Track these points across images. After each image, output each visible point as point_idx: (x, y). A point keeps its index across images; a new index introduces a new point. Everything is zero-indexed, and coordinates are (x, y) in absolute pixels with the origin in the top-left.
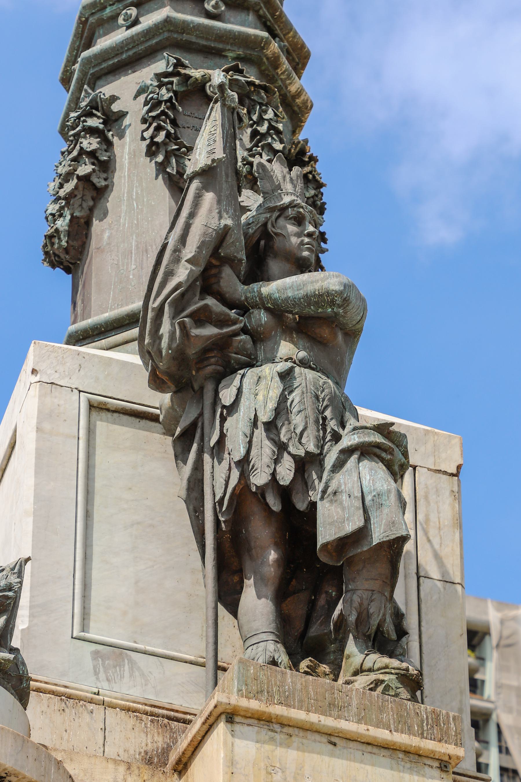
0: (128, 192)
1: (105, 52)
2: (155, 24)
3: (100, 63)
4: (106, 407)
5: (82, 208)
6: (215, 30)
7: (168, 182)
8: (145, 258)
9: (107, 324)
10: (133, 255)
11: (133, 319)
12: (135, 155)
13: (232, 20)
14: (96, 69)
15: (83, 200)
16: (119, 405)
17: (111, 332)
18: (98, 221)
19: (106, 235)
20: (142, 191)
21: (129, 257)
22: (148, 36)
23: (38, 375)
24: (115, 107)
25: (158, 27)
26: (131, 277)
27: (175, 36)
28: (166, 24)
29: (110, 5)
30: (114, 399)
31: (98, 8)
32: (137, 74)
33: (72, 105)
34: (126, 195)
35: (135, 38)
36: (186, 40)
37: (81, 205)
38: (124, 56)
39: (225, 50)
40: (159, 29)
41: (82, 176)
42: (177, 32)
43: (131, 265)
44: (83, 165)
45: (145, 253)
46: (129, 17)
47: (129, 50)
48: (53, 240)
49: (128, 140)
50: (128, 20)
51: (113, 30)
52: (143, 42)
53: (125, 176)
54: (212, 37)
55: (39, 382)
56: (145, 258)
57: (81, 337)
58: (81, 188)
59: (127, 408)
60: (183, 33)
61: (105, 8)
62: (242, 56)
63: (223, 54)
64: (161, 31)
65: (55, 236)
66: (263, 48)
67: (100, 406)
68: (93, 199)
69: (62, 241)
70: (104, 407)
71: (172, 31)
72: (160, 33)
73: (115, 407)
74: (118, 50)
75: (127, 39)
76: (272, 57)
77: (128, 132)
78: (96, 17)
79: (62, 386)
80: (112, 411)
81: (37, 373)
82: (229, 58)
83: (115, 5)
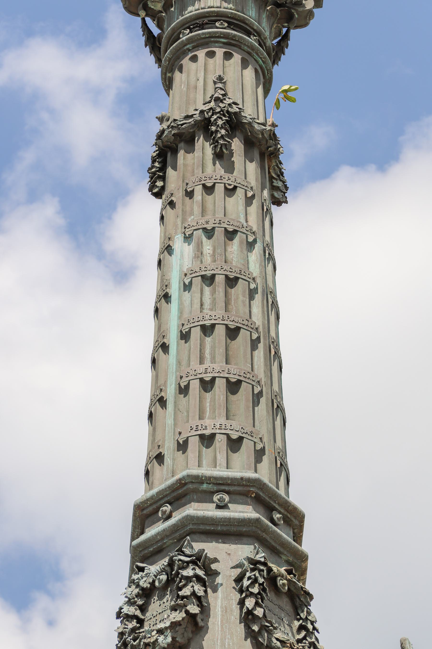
0: (221, 639)
2: (249, 519)
20: (233, 644)
22: (240, 524)
27: (260, 532)
28: (257, 522)
29: (207, 483)
31: (198, 481)
33: (158, 537)
34: (219, 642)
35: (231, 520)
37: (183, 634)
38: (219, 528)
39: (283, 554)
40: (250, 523)
41: (191, 614)
42: (261, 530)
46: (223, 500)
49: (220, 595)
54: (279, 542)
58: (186, 621)
60: (263, 532)
61: (203, 483)
63: (280, 555)
64: (251, 525)
68: (193, 632)
71: (258, 528)
72: (250, 526)
74: (216, 522)
75: (226, 518)
76: (304, 568)
77: (220, 589)
78: (195, 486)
82: (283, 559)
83: (211, 485)
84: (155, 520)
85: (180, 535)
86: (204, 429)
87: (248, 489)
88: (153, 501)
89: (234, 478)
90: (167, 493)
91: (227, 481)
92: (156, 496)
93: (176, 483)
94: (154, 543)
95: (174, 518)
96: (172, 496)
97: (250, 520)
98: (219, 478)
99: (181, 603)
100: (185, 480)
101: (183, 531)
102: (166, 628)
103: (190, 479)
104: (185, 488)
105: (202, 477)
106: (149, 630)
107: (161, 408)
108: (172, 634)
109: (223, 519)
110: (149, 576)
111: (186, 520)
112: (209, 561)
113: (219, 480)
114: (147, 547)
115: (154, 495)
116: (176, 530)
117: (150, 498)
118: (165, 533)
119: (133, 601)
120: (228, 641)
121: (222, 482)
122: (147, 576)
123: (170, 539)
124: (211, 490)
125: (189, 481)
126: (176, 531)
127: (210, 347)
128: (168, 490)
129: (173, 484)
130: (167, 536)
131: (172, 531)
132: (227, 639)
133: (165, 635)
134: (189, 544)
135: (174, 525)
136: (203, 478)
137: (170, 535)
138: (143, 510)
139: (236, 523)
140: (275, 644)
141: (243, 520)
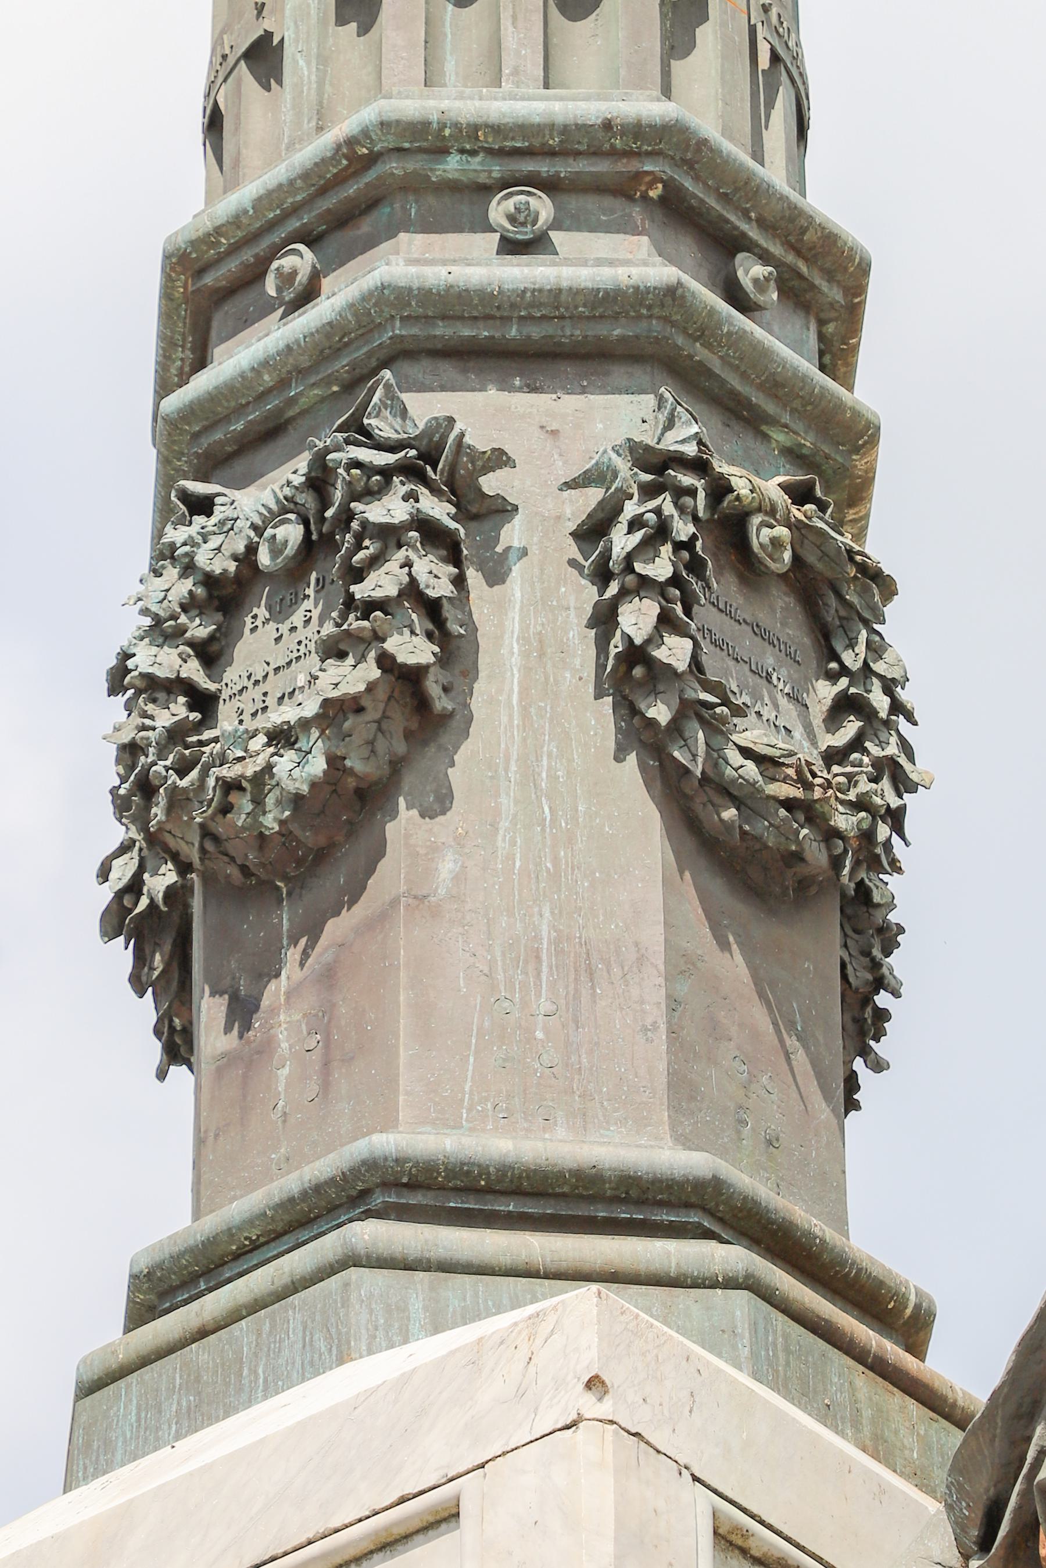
1: (459, 295)
2: (637, 288)
3: (426, 317)
4: (744, 1545)
5: (373, 751)
6: (772, 361)
7: (658, 784)
8: (585, 993)
9: (505, 1175)
10: (545, 969)
11: (585, 1188)
12: (542, 655)
13: (776, 328)
14: (415, 331)
15: (380, 729)
16: (776, 1547)
17: (503, 1199)
18: (415, 812)
19: (447, 867)
21: (531, 968)
22: (601, 310)
23: (608, 1401)
24: (490, 483)
25: (643, 299)
26: (539, 1035)
27: (680, 340)
28: (668, 301)
29: (462, 151)
30: (762, 1522)
32: (543, 400)
33: (266, 377)
34: (513, 767)
36: (700, 362)
37: (371, 743)
38: (513, 332)
40: (641, 305)
42: (684, 331)
43: (539, 995)
44: (406, 631)
45: (584, 977)
50: (523, 224)
51: (458, 228)
53: (510, 706)
55: (612, 1422)
56: (585, 993)
57: (405, 1180)
58: (382, 694)
59: (790, 1562)
60: (696, 339)
61: (444, 151)
62: (804, 451)
63: (764, 428)
64: (644, 311)
65: (243, 789)
66: (857, 450)
67: (733, 1538)
68: (408, 735)
69: (264, 813)
70: (740, 1542)
71: (673, 324)
72: (639, 317)
73: (765, 1549)
74: (498, 308)
76: (860, 477)
78: (412, 165)
79: (658, 1452)
80: (752, 1557)
81: (606, 1392)
82: (774, 445)
88: (240, 234)
89: (576, 125)
90: (299, 198)
92: (251, 212)
93: (333, 158)
94: (248, 403)
98: (511, 129)
101: (365, 349)
104: (371, 176)
106: (239, 734)
108: (328, 743)
109: (528, 294)
111: (375, 305)
113: (511, 135)
115: (245, 212)
118: (291, 360)
121: (527, 144)
122: (225, 529)
123: (314, 384)
124: (480, 181)
125: (386, 144)
126: (337, 351)
128: (302, 188)
129: (322, 163)
130: (302, 372)
131: (322, 352)
132: (545, 758)
134: (392, 400)
135: (328, 328)
138: (201, 272)
141: (611, 294)
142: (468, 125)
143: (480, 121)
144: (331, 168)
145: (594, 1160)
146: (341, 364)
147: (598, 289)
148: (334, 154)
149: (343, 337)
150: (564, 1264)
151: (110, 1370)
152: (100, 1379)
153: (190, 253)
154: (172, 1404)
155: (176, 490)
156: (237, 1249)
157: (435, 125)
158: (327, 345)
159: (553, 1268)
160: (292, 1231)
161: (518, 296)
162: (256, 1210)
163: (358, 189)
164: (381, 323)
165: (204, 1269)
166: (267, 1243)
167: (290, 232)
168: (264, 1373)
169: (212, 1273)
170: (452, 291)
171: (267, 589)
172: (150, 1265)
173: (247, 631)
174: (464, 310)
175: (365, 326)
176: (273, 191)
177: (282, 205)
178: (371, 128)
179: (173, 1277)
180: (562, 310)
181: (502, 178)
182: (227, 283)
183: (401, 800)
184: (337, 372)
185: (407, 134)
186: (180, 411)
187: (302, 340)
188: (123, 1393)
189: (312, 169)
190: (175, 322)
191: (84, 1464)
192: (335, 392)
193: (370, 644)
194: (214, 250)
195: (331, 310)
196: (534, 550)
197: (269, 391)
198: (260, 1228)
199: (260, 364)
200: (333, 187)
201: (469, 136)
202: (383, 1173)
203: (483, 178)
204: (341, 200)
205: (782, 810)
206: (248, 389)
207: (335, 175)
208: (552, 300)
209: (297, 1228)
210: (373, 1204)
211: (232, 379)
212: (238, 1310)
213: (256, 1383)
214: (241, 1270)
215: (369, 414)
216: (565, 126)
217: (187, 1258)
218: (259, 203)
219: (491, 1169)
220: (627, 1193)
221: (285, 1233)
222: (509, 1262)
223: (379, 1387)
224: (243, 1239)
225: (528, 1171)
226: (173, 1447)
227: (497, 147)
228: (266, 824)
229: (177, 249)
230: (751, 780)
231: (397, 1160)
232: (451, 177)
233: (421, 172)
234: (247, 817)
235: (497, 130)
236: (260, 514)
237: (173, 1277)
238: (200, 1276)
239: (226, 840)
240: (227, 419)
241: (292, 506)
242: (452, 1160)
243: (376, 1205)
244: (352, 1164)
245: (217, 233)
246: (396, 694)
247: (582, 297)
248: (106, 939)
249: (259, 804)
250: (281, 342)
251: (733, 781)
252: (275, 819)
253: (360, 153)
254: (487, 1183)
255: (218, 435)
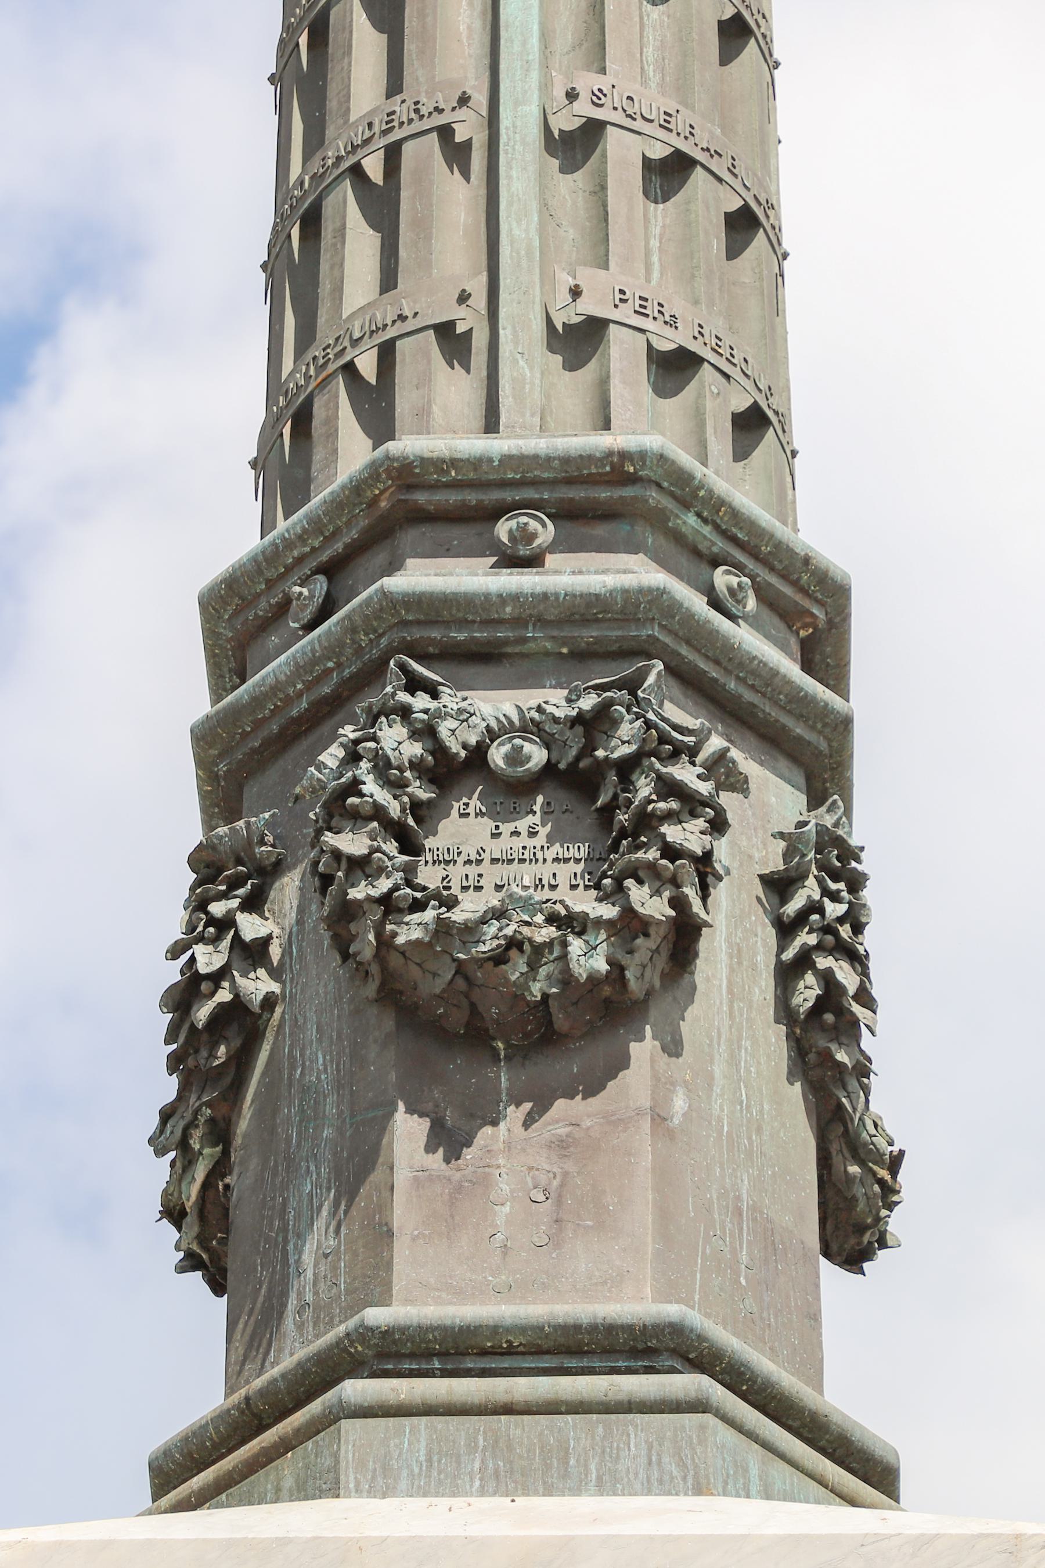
9: (765, 1390)
22: (794, 706)
25: (826, 716)
29: (699, 515)
31: (679, 492)
33: (508, 609)
35: (777, 680)
37: (644, 967)
47: (741, 680)
48: (404, 905)
52: (776, 703)
64: (819, 726)
68: (663, 976)
69: (534, 980)
74: (730, 659)
75: (765, 664)
78: (667, 503)
84: (456, 542)
85: (598, 641)
86: (666, 323)
87: (806, 603)
88: (472, 475)
89: (788, 546)
90: (546, 475)
91: (764, 543)
92: (496, 463)
93: (600, 460)
94: (474, 622)
95: (573, 573)
96: (561, 496)
97: (828, 711)
98: (744, 521)
99: (666, 868)
100: (644, 463)
101: (619, 633)
102: (599, 922)
103: (660, 471)
104: (628, 492)
105: (701, 487)
106: (532, 902)
107: (447, 164)
108: (612, 949)
109: (756, 662)
110: (466, 720)
111: (649, 602)
112: (727, 776)
113: (741, 525)
114: (437, 622)
115: (490, 460)
116: (589, 617)
117: (468, 460)
118: (542, 607)
119: (395, 774)
120: (746, 1057)
121: (746, 539)
122: (461, 718)
123: (553, 637)
124: (700, 547)
125: (652, 474)
126: (586, 621)
127: (658, 44)
128: (555, 469)
129: (587, 459)
130: (541, 622)
131: (573, 614)
132: (743, 1051)
133: (587, 942)
134: (658, 688)
135: (593, 599)
136: (702, 493)
137: (559, 623)
138: (411, 487)
139: (781, 697)
140: (871, 1136)
141: (809, 698)
142: (719, 497)
143: (727, 499)
144: (593, 467)
145: (827, 1410)
146: (589, 634)
147: (802, 688)
148: (604, 458)
149: (600, 613)
150: (846, 1489)
151: (386, 1404)
152: (370, 1407)
153: (416, 467)
154: (473, 1460)
155: (395, 660)
156: (491, 1347)
157: (697, 482)
158: (582, 611)
159: (838, 1488)
160: (555, 1354)
161: (749, 659)
162: (533, 1321)
163: (611, 497)
164: (639, 619)
165: (443, 1350)
166: (523, 1353)
167: (524, 499)
168: (597, 1470)
169: (448, 1357)
170: (707, 625)
171: (481, 787)
172: (391, 1325)
173: (454, 813)
174: (706, 646)
175: (625, 614)
176: (527, 457)
177: (528, 473)
178: (649, 454)
179: (409, 1344)
180: (769, 689)
181: (717, 554)
182: (434, 509)
183: (648, 1027)
184: (582, 638)
185: (674, 476)
186: (406, 595)
187: (562, 596)
188: (408, 1431)
189: (575, 458)
190: (342, 515)
191: (356, 1478)
192: (561, 653)
193: (663, 884)
194: (438, 476)
195: (602, 585)
196: (734, 872)
197: (500, 622)
198: (529, 1338)
199: (509, 595)
200: (582, 483)
201: (714, 506)
202: (683, 1341)
203: (703, 547)
204: (589, 498)
205: (876, 1185)
206: (484, 609)
207: (590, 475)
208: (768, 677)
209: (562, 1353)
210: (661, 1364)
211: (474, 594)
212: (557, 1403)
213: (586, 1475)
214: (488, 1366)
215: (645, 689)
216: (780, 542)
217: (436, 1334)
218: (507, 460)
219: (759, 1380)
220: (834, 1450)
221: (548, 1352)
222: (810, 1468)
223: (892, 1536)
224: (504, 1341)
225: (782, 1394)
226: (513, 1501)
227: (724, 527)
228: (533, 989)
229: (404, 458)
230: (881, 1151)
231: (699, 1336)
232: (683, 530)
233: (667, 512)
234: (521, 976)
235: (735, 514)
236: (497, 719)
237: (409, 1344)
238: (435, 1355)
239: (479, 986)
240: (447, 624)
241: (535, 730)
242: (736, 1357)
243: (663, 1366)
244: (658, 1322)
245: (452, 464)
246: (670, 937)
247: (789, 688)
248: (165, 1010)
249: (532, 969)
250: (538, 588)
251: (865, 1144)
252: (541, 989)
253: (626, 469)
254: (747, 1389)
255: (435, 634)
